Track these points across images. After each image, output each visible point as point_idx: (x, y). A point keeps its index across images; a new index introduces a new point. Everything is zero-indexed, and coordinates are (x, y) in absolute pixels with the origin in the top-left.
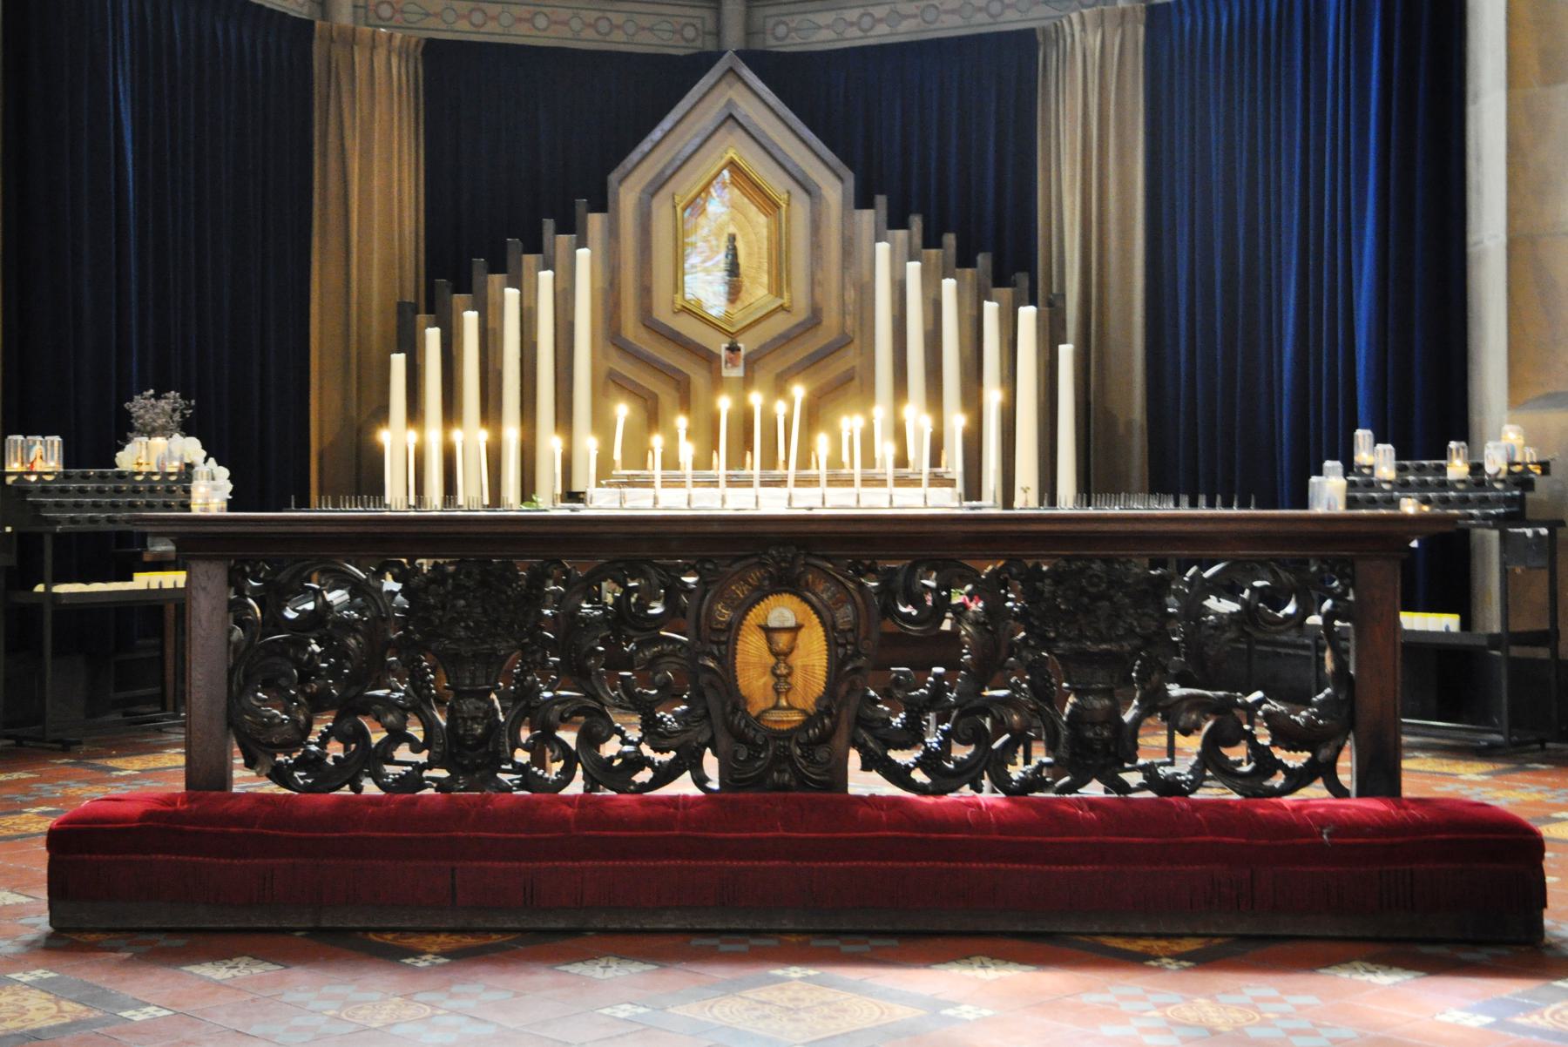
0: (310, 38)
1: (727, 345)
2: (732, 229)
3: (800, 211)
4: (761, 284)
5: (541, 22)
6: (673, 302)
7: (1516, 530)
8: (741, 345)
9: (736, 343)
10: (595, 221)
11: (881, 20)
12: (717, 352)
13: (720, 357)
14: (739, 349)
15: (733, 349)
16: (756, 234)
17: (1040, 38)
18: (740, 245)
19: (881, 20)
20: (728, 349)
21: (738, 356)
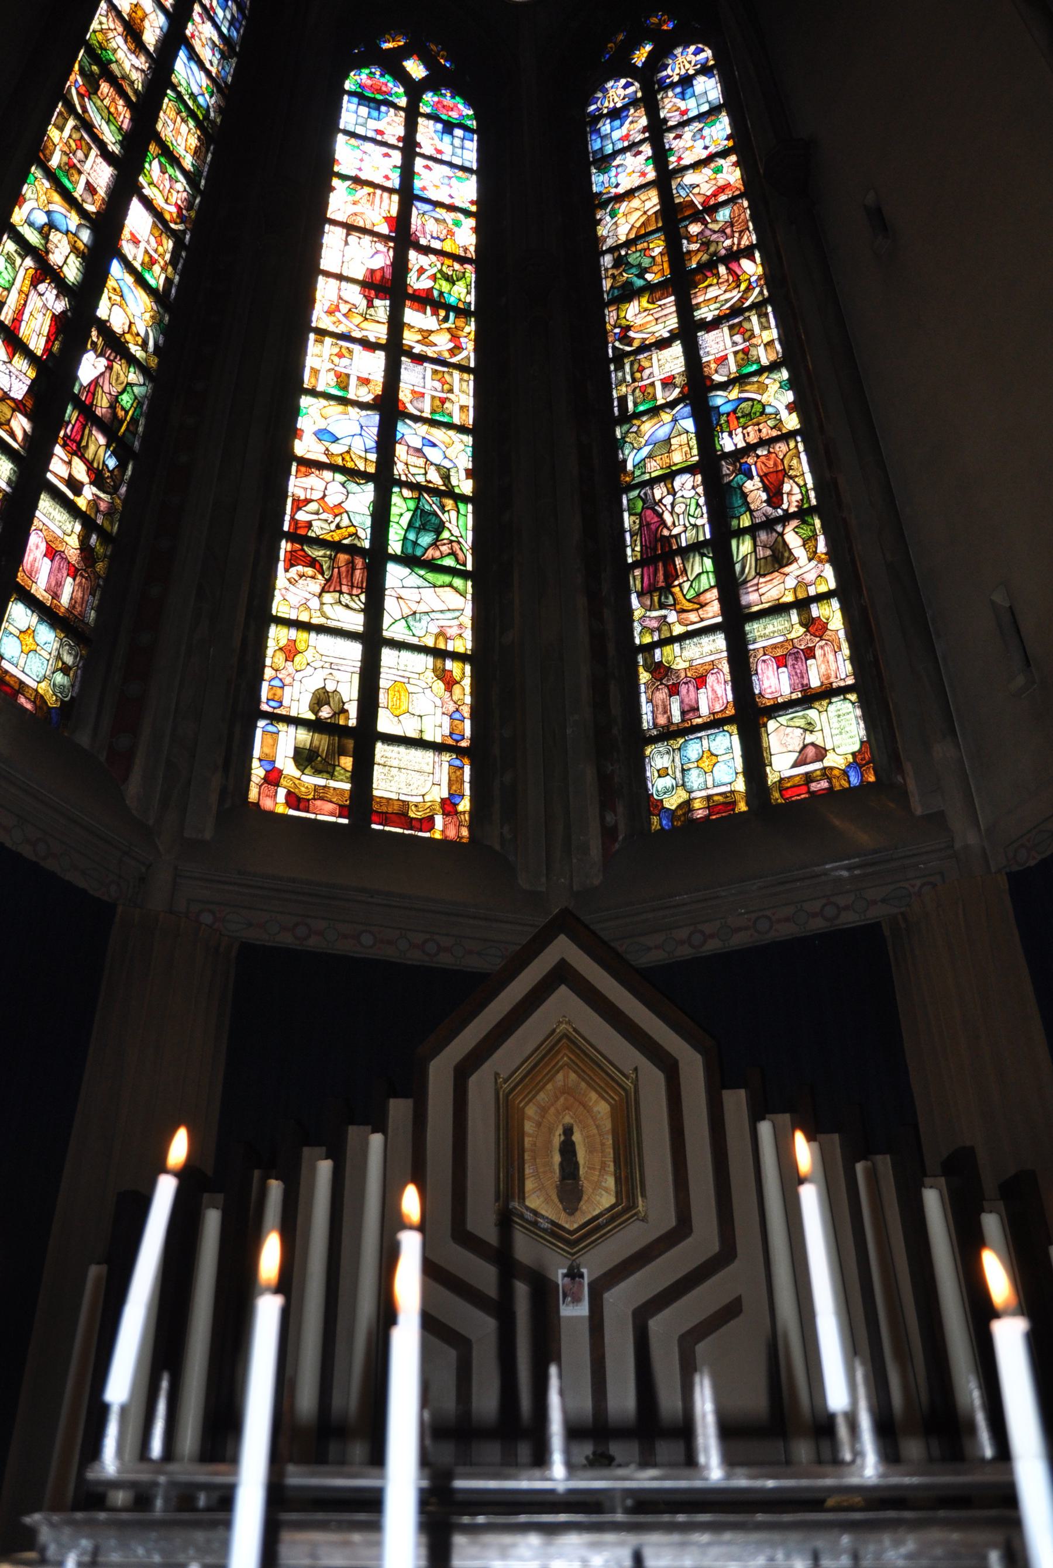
0: (611, 1513)
1: (565, 1271)
2: (568, 1119)
3: (653, 1080)
4: (606, 1190)
5: (366, 939)
6: (193, 24)
7: (907, 1480)
8: (584, 1271)
9: (578, 1268)
10: (399, 1109)
11: (712, 936)
12: (554, 1279)
13: (558, 1285)
14: (581, 1276)
15: (574, 1274)
16: (598, 1127)
17: (887, 932)
18: (577, 1137)
19: (712, 936)
20: (565, 1276)
21: (581, 1285)
